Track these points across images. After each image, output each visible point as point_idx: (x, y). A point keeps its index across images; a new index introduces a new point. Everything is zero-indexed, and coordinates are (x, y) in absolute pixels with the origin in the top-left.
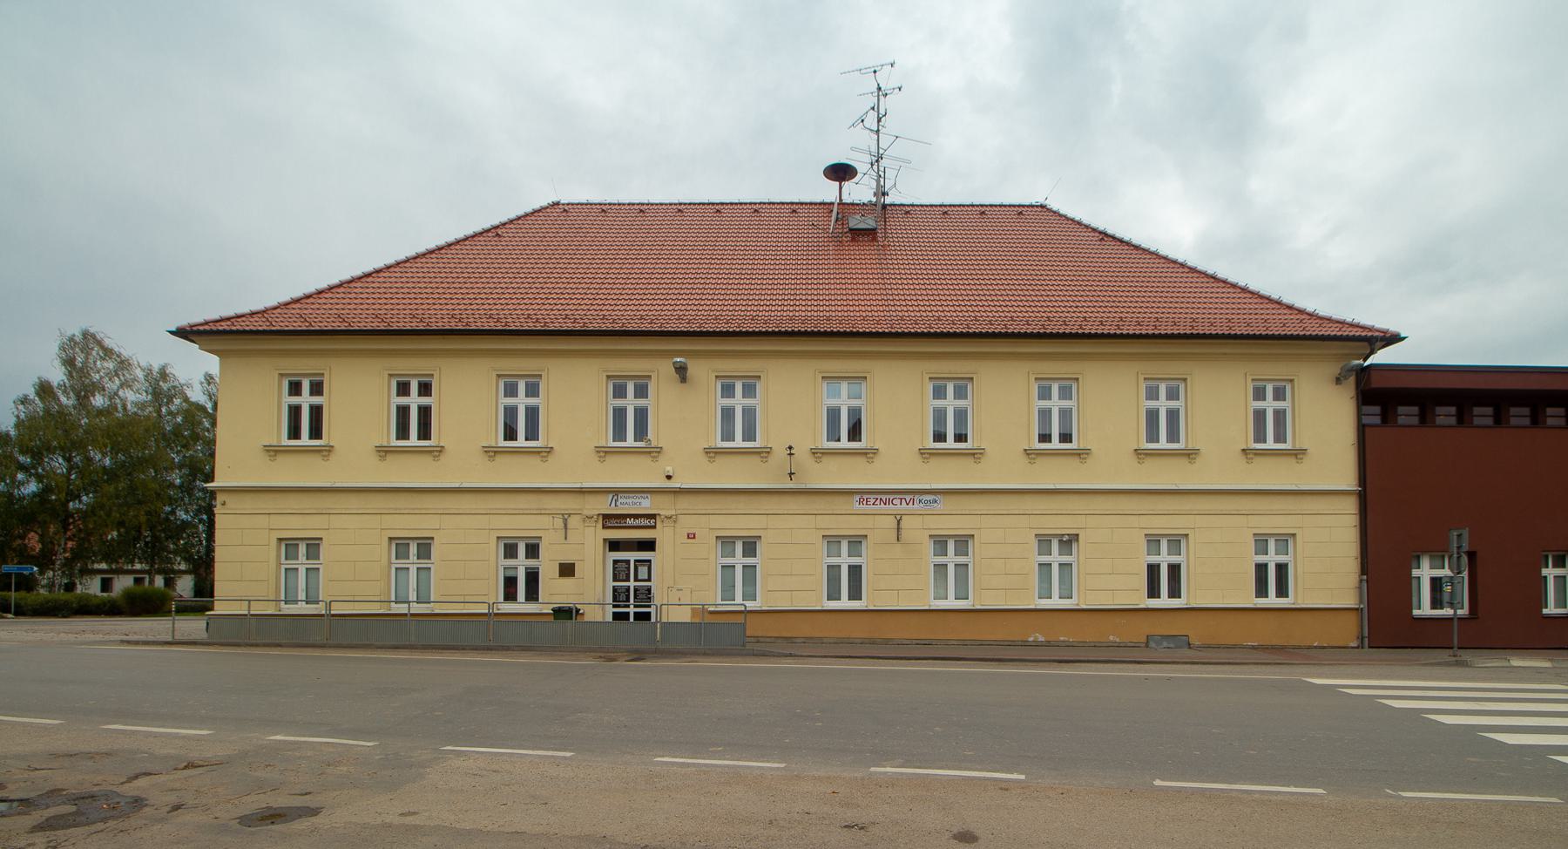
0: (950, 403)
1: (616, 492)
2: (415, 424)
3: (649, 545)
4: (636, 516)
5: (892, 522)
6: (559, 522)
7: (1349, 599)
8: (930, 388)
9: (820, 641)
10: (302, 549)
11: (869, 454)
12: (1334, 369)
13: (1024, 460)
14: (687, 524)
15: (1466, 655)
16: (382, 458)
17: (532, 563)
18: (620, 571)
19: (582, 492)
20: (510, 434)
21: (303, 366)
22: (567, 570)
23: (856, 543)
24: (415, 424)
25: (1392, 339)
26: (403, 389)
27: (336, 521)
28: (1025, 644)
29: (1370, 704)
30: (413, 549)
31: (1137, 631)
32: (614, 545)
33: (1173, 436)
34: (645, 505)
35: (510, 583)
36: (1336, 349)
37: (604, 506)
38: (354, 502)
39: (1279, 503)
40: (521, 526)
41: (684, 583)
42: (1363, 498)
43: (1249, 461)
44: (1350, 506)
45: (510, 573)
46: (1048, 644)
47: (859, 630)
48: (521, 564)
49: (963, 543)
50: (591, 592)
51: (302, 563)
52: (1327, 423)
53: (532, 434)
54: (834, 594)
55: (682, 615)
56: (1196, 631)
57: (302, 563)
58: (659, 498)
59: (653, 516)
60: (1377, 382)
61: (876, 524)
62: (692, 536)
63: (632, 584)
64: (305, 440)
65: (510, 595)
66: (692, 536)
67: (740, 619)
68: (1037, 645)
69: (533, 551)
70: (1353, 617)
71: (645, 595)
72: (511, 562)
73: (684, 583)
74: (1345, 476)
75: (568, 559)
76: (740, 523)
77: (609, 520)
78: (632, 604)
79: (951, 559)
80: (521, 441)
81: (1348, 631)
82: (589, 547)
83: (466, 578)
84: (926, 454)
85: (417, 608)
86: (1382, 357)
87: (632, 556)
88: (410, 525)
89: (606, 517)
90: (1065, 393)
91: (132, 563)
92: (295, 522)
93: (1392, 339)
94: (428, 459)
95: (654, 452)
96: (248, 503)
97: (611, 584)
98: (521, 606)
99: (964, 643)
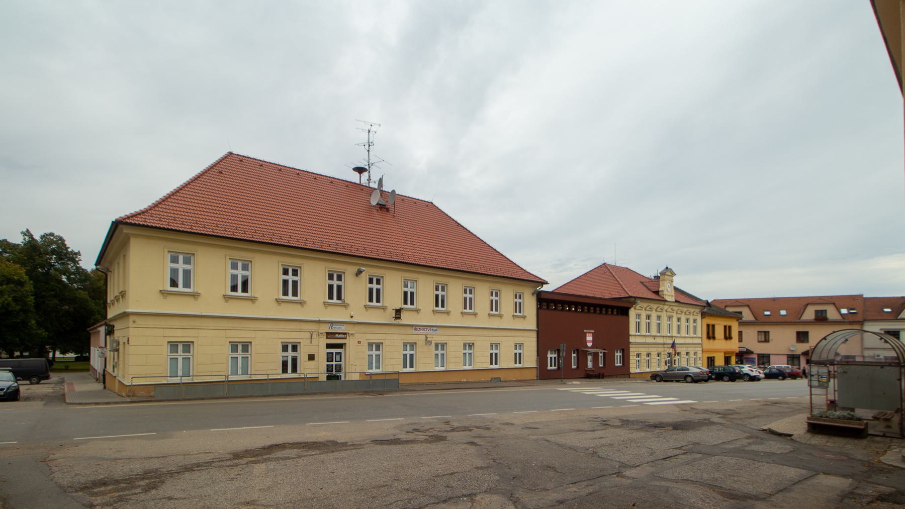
0: (181, 266)
1: (332, 323)
2: (290, 288)
3: (340, 346)
4: (339, 333)
5: (424, 338)
6: (308, 335)
7: (534, 365)
8: (168, 256)
9: (423, 384)
10: (180, 347)
11: (253, 300)
12: (532, 291)
13: (275, 304)
14: (358, 337)
15: (564, 381)
16: (279, 304)
17: (294, 354)
18: (330, 358)
19: (319, 322)
20: (174, 283)
21: (292, 262)
22: (311, 357)
23: (413, 345)
24: (290, 288)
25: (546, 283)
26: (286, 272)
27: (202, 333)
28: (461, 383)
29: (579, 394)
30: (240, 348)
31: (487, 377)
32: (329, 346)
33: (187, 284)
34: (343, 329)
35: (285, 364)
36: (534, 284)
37: (326, 328)
38: (151, 322)
39: (512, 332)
40: (291, 337)
41: (356, 364)
42: (538, 332)
43: (227, 301)
44: (534, 334)
45: (285, 359)
46: (467, 382)
47: (414, 380)
48: (290, 354)
49: (187, 346)
50: (316, 369)
51: (240, 354)
52: (530, 306)
53: (187, 284)
54: (405, 366)
55: (356, 377)
56: (502, 376)
57: (240, 354)
58: (350, 326)
59: (345, 334)
60: (543, 296)
61: (419, 339)
62: (359, 342)
63: (334, 363)
64: (335, 300)
65: (285, 370)
66: (359, 342)
67: (396, 377)
68: (464, 383)
69: (295, 348)
70: (535, 370)
71: (339, 368)
72: (285, 354)
73: (356, 364)
74: (533, 325)
75: (312, 352)
76: (376, 338)
77: (329, 335)
78: (333, 374)
79: (180, 355)
80: (181, 288)
81: (533, 375)
82: (320, 348)
83: (266, 363)
84: (226, 298)
85: (185, 380)
86: (545, 288)
87: (334, 351)
88: (241, 336)
89: (328, 333)
90: (187, 261)
91: (42, 353)
92: (179, 333)
93: (546, 283)
94: (191, 299)
95: (346, 306)
96: (140, 321)
97: (342, 363)
98: (290, 375)
99: (445, 383)
